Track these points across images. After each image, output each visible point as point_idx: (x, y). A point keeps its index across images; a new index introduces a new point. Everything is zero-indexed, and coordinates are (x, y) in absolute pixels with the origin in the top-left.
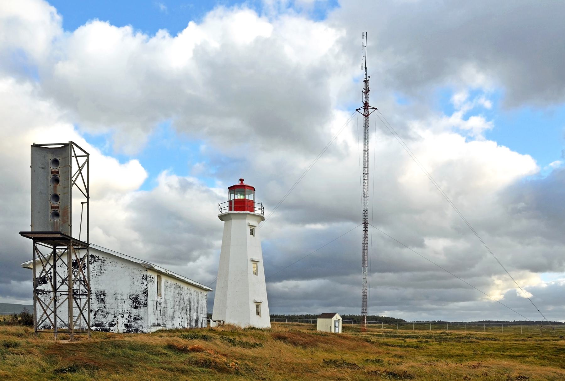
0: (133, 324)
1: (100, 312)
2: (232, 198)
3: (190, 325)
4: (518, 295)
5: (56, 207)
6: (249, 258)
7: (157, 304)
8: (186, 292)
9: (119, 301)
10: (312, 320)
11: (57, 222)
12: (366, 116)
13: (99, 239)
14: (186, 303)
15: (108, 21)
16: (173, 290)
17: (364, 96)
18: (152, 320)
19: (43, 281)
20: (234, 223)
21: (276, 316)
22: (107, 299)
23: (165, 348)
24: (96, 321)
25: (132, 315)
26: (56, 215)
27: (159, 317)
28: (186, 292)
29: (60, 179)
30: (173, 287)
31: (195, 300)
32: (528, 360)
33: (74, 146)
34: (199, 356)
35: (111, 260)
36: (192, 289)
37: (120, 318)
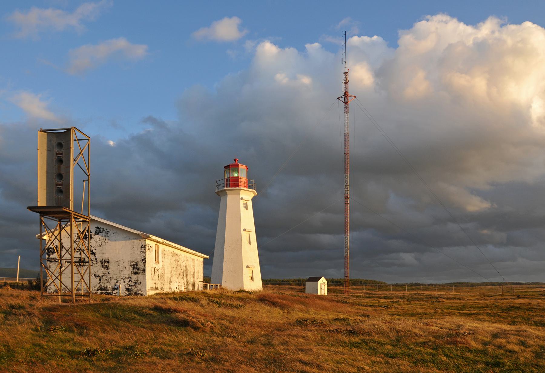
1: (104, 278)
3: (187, 288)
5: (60, 185)
9: (121, 268)
14: (183, 269)
15: (400, 32)
16: (170, 257)
21: (266, 281)
22: (111, 266)
24: (101, 286)
26: (61, 191)
27: (157, 281)
29: (63, 159)
30: (171, 254)
31: (192, 267)
32: (481, 317)
35: (114, 232)
37: (122, 282)
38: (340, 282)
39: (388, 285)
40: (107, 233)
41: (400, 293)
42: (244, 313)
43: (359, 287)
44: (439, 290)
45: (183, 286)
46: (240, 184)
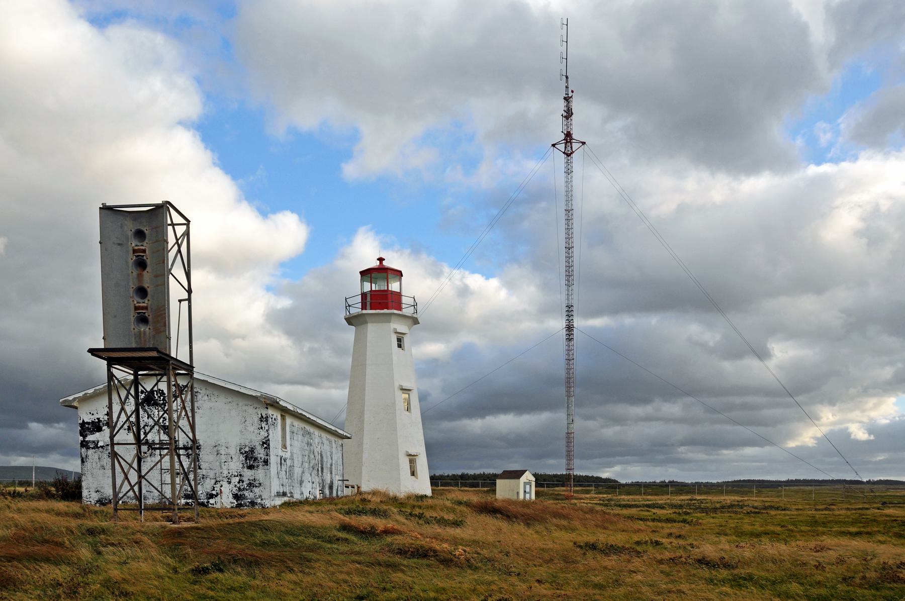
0: (246, 493)
2: (367, 287)
4: (853, 437)
5: (143, 308)
6: (397, 385)
7: (282, 460)
8: (317, 440)
9: (223, 458)
10: (489, 481)
11: (145, 332)
12: (568, 155)
13: (208, 356)
16: (300, 437)
17: (565, 123)
18: (276, 487)
19: (96, 427)
20: (372, 329)
21: (442, 477)
23: (339, 530)
25: (244, 479)
26: (143, 320)
27: (285, 481)
28: (317, 440)
29: (148, 262)
30: (301, 433)
31: (329, 454)
33: (171, 209)
34: (398, 540)
35: (208, 392)
36: (325, 435)
37: (225, 484)
45: (318, 489)
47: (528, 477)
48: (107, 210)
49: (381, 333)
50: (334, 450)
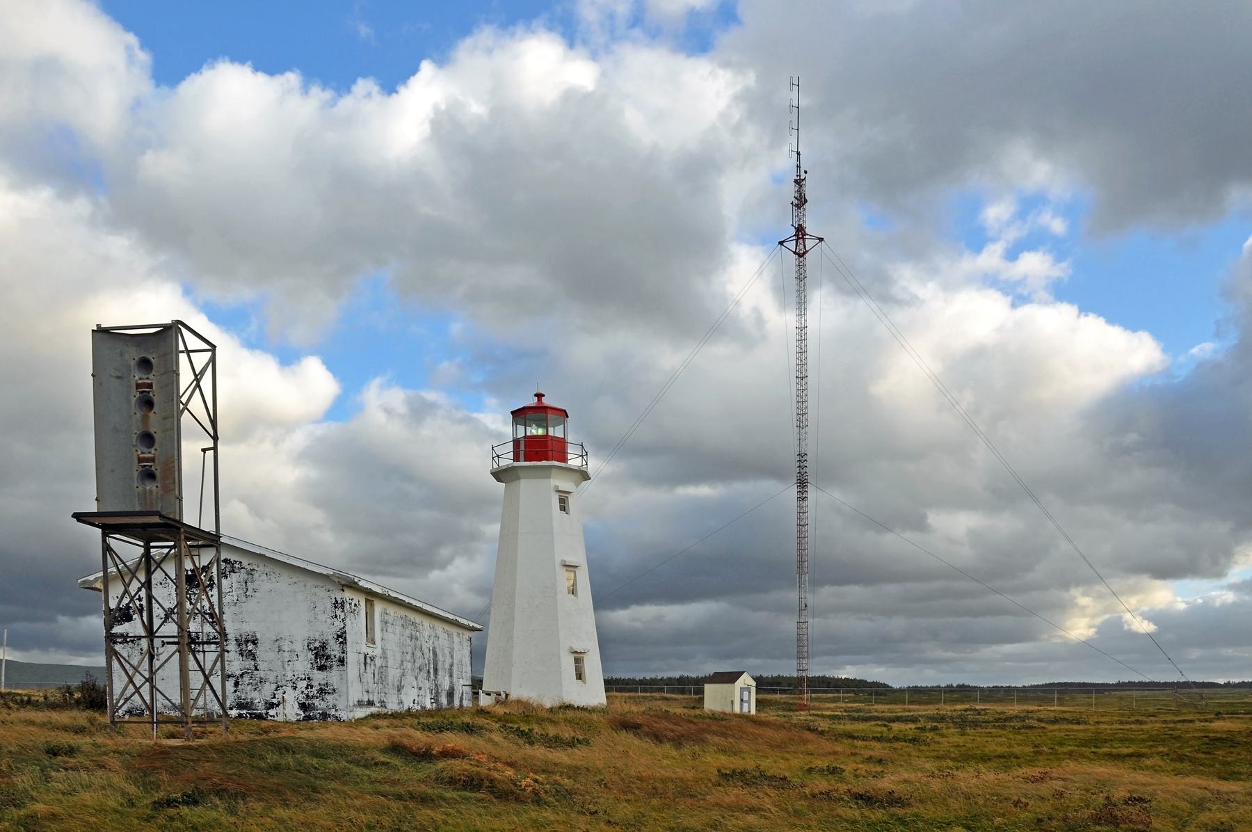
0: (316, 702)
1: (246, 679)
3: (437, 701)
5: (148, 460)
6: (558, 560)
7: (367, 660)
8: (426, 634)
9: (287, 656)
10: (692, 687)
11: (151, 491)
12: (801, 256)
13: (240, 524)
14: (427, 657)
15: (249, 63)
16: (398, 629)
17: (795, 213)
19: (125, 615)
20: (527, 487)
21: (617, 681)
22: (261, 652)
24: (239, 698)
25: (313, 683)
26: (150, 476)
27: (372, 686)
28: (426, 634)
29: (156, 400)
30: (400, 622)
31: (447, 651)
33: (184, 330)
35: (267, 570)
36: (440, 627)
37: (289, 689)
38: (778, 684)
39: (894, 691)
40: (251, 573)
41: (931, 710)
42: (594, 755)
43: (825, 695)
44: (1022, 700)
45: (429, 696)
46: (550, 453)
47: (746, 680)
48: (102, 334)
49: (537, 490)
50: (456, 646)
